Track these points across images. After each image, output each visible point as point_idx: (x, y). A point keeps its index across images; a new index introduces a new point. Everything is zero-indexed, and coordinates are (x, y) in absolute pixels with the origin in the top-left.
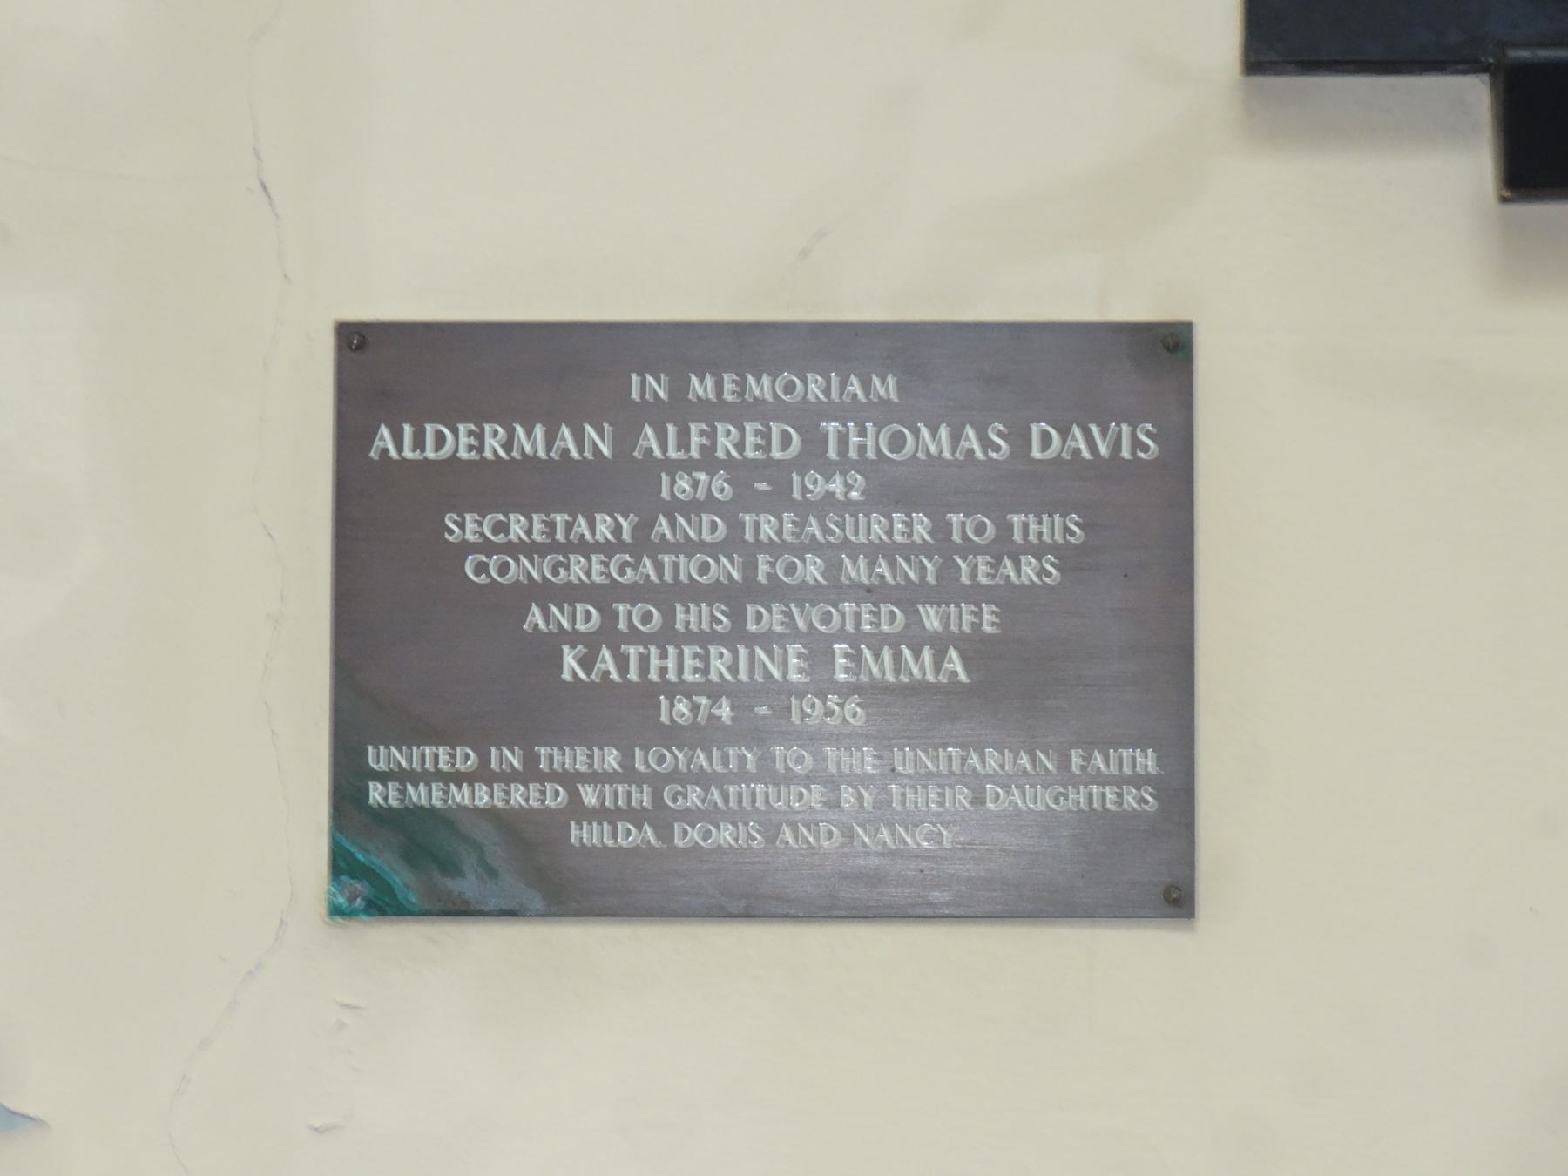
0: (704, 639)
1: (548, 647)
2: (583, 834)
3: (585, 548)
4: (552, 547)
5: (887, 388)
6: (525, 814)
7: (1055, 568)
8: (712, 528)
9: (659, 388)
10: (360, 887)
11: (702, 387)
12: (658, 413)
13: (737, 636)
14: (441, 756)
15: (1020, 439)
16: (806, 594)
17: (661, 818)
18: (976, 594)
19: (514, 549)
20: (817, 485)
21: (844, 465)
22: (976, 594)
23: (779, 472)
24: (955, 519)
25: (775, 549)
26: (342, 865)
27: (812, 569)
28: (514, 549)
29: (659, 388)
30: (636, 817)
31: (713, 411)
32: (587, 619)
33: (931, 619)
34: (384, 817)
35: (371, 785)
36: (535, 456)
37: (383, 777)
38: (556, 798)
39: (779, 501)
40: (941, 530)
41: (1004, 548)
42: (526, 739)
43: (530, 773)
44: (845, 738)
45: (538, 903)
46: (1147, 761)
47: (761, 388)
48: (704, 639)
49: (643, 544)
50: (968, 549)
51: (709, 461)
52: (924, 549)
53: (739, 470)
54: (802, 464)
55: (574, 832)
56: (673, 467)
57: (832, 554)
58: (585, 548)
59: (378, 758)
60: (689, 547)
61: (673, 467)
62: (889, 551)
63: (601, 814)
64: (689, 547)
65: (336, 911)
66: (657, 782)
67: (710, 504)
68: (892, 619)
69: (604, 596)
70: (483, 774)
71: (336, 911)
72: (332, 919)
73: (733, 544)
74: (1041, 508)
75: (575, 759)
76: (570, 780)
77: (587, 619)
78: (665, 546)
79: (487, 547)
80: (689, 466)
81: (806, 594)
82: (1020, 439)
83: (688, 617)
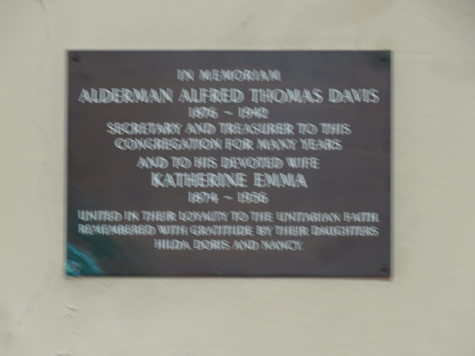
0: (205, 171)
1: (147, 173)
2: (161, 244)
3: (161, 136)
4: (151, 136)
5: (275, 75)
6: (139, 237)
7: (340, 144)
8: (209, 128)
9: (189, 75)
10: (77, 264)
11: (205, 75)
12: (188, 85)
13: (219, 170)
14: (106, 215)
15: (325, 95)
16: (245, 154)
17: (190, 238)
18: (309, 154)
19: (134, 136)
20: (248, 112)
21: (260, 105)
22: (309, 154)
23: (233, 107)
24: (301, 125)
25: (232, 136)
26: (70, 256)
27: (247, 144)
28: (134, 136)
29: (189, 75)
30: (180, 238)
31: (209, 84)
32: (162, 163)
33: (292, 162)
34: (86, 238)
35: (79, 225)
36: (362, 101)
37: (84, 223)
38: (149, 230)
39: (234, 119)
40: (296, 129)
41: (320, 136)
42: (138, 210)
43: (142, 222)
44: (260, 207)
45: (96, 268)
46: (373, 217)
47: (228, 75)
48: (205, 171)
49: (184, 135)
50: (307, 136)
51: (209, 104)
52: (290, 137)
53: (220, 107)
54: (243, 105)
55: (156, 243)
56: (194, 105)
57: (254, 138)
58: (161, 136)
59: (84, 215)
60: (201, 136)
61: (194, 105)
62: (275, 137)
63: (169, 237)
64: (201, 136)
65: (69, 274)
66: (188, 224)
67: (210, 120)
68: (277, 163)
69: (167, 154)
70: (124, 222)
71: (69, 274)
72: (68, 277)
73: (219, 135)
74: (332, 121)
75: (157, 216)
76: (155, 224)
77: (162, 163)
78: (193, 136)
79: (125, 136)
80: (200, 105)
81: (245, 154)
82: (325, 95)
83: (201, 162)
